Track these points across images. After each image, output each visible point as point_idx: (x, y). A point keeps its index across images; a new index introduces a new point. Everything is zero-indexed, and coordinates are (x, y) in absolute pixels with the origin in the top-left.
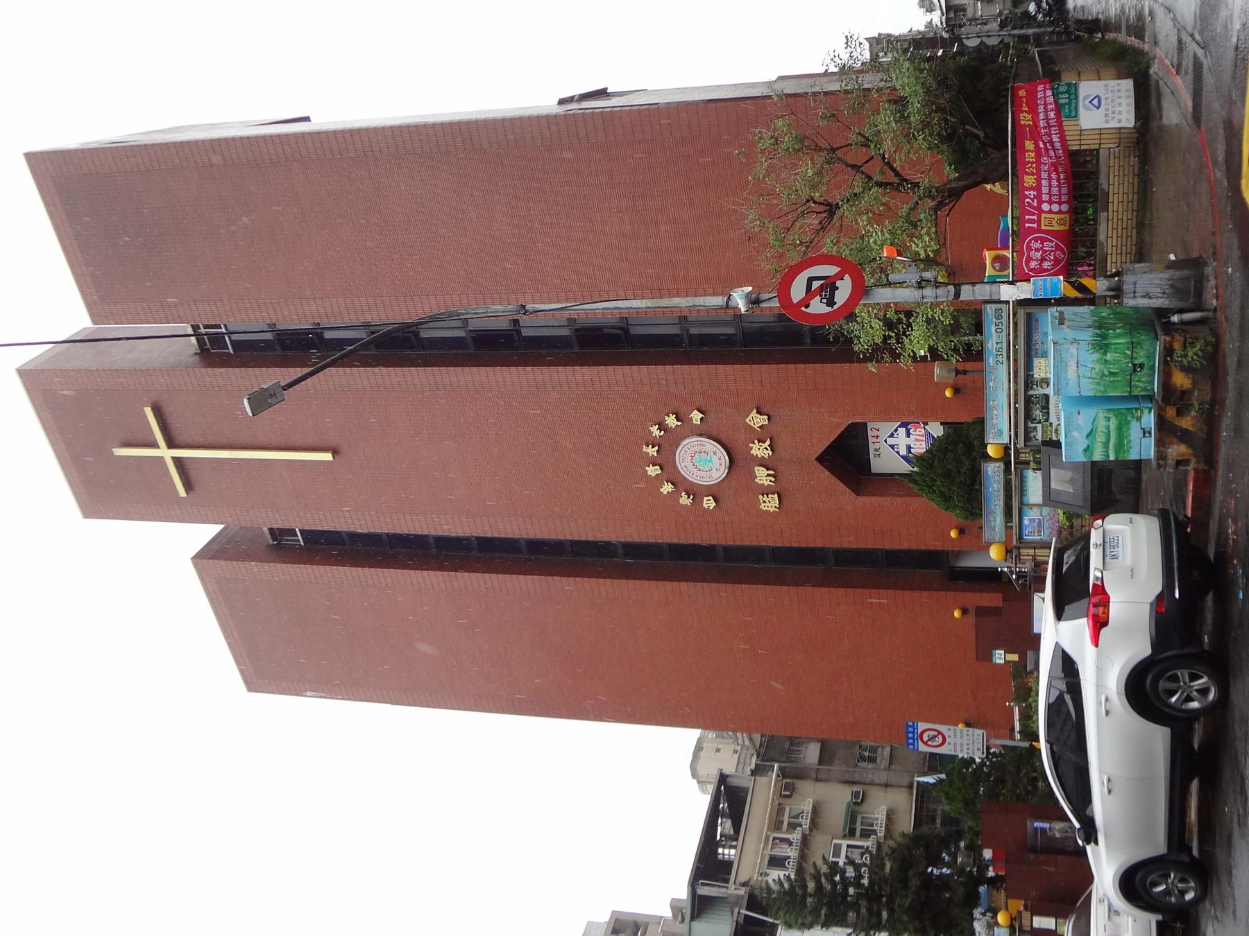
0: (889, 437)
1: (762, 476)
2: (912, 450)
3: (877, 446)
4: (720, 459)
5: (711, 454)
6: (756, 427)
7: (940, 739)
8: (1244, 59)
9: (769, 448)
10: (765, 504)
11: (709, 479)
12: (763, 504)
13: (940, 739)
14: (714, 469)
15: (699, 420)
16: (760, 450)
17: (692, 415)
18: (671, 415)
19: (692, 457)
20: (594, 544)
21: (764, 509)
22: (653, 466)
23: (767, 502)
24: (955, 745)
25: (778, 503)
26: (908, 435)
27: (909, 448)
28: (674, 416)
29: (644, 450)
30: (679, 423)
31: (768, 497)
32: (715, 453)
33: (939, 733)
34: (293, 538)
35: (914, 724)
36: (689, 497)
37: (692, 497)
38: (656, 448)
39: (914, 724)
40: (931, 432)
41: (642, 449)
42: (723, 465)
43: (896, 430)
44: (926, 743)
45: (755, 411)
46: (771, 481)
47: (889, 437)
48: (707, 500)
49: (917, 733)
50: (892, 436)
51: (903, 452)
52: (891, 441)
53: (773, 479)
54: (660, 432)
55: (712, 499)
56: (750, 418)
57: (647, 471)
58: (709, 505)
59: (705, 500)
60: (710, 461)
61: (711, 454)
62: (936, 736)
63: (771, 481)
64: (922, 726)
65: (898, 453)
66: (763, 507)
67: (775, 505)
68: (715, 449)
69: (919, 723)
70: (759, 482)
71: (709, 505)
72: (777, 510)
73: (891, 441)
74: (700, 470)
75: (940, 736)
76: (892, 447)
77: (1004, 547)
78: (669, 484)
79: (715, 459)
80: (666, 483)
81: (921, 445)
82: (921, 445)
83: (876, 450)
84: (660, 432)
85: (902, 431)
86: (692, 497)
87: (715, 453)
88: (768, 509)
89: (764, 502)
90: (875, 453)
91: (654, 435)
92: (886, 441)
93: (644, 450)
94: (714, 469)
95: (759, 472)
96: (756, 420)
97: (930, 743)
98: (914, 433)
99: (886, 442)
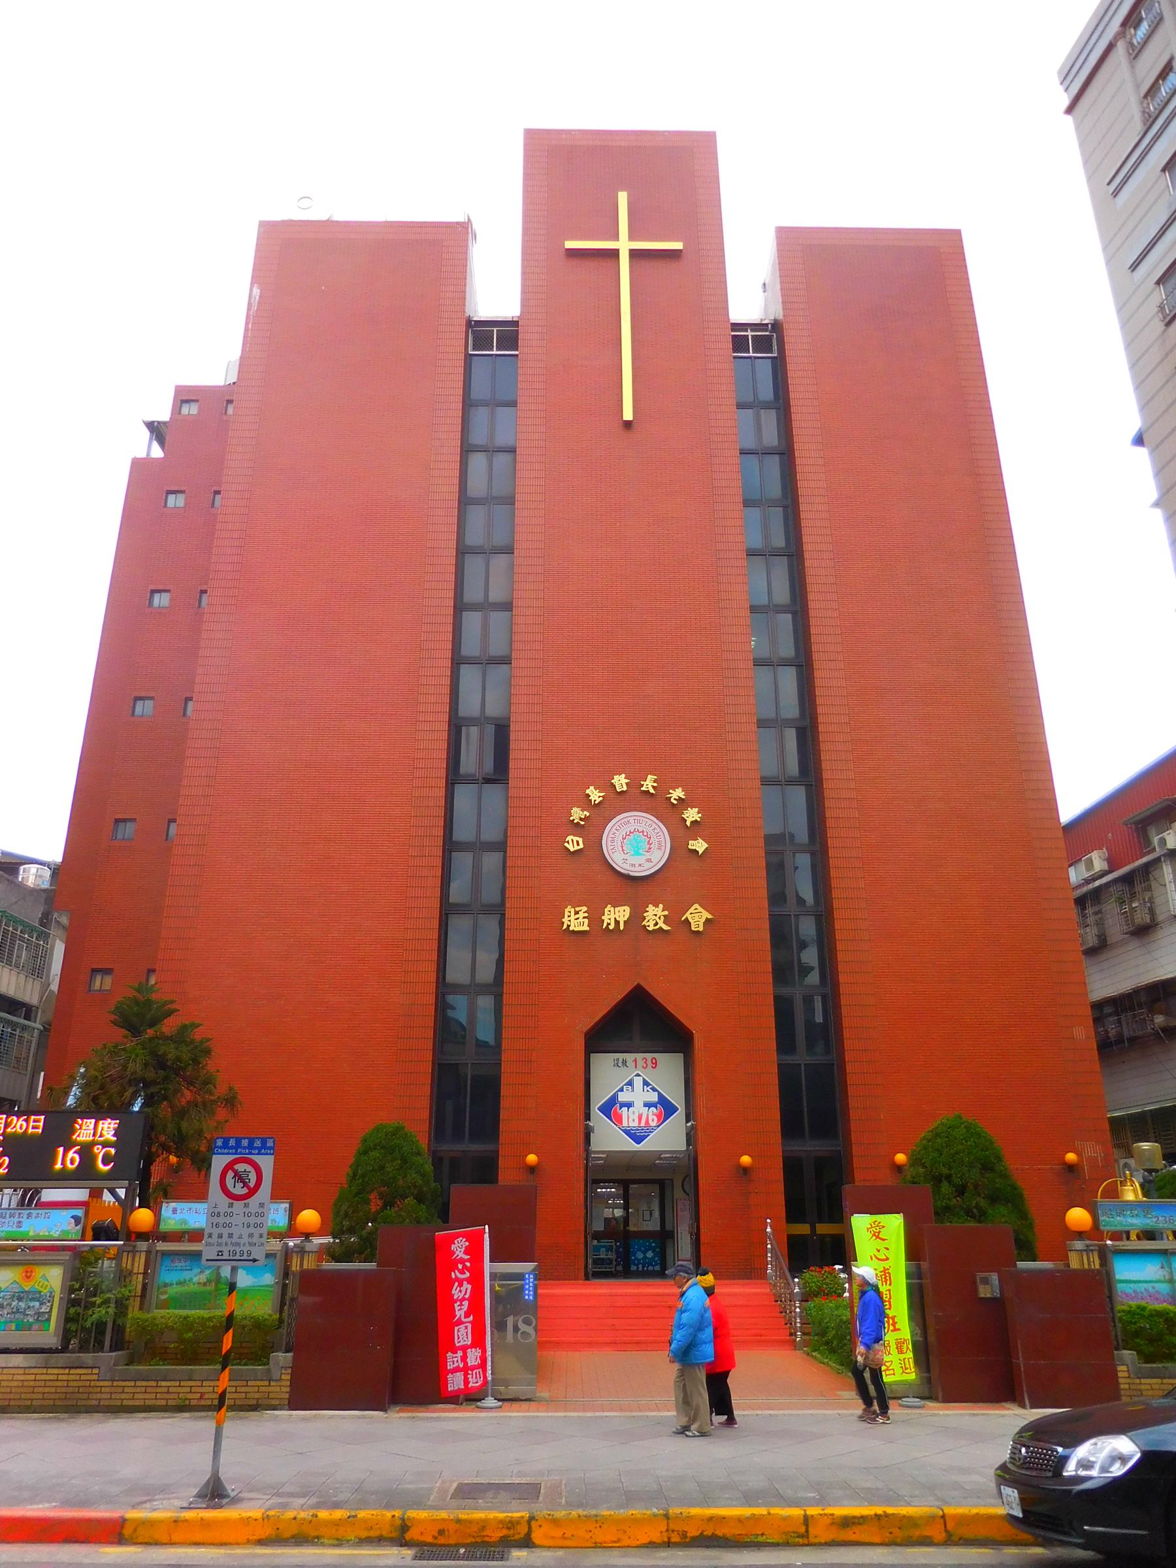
0: (643, 1079)
1: (616, 915)
2: (625, 1109)
3: (630, 1063)
4: (640, 865)
5: (648, 856)
6: (687, 915)
7: (239, 1190)
8: (596, 1543)
9: (657, 927)
10: (573, 913)
11: (610, 848)
12: (573, 911)
13: (239, 1190)
14: (626, 857)
15: (694, 848)
16: (654, 916)
17: (700, 840)
18: (700, 815)
19: (643, 832)
20: (812, 870)
21: (566, 910)
22: (627, 784)
23: (577, 916)
24: (231, 1215)
25: (576, 929)
26: (648, 1105)
27: (629, 1105)
28: (699, 820)
29: (650, 777)
30: (688, 823)
31: (584, 918)
32: (649, 860)
33: (252, 1192)
34: (1138, 853)
35: (270, 1148)
36: (581, 819)
37: (582, 823)
38: (652, 791)
39: (270, 1148)
40: (652, 1135)
41: (651, 774)
42: (633, 869)
43: (654, 1089)
44: (229, 1166)
45: (710, 916)
46: (609, 924)
47: (643, 1079)
48: (578, 842)
49: (250, 1153)
50: (646, 1083)
51: (622, 1097)
52: (638, 1082)
53: (611, 927)
54: (675, 799)
55: (579, 848)
56: (700, 909)
57: (620, 774)
58: (570, 842)
59: (578, 839)
60: (637, 853)
61: (648, 856)
62: (245, 1185)
63: (609, 924)
64: (266, 1163)
65: (621, 1090)
66: (569, 910)
67: (572, 925)
68: (655, 861)
69: (273, 1157)
70: (606, 910)
71: (570, 842)
72: (565, 927)
73: (638, 1082)
74: (623, 839)
75: (245, 1191)
76: (630, 1083)
77: (314, 1231)
78: (601, 798)
79: (637, 860)
80: (602, 794)
81: (634, 1120)
82: (634, 1120)
83: (624, 1063)
84: (675, 799)
85: (654, 1097)
86: (582, 823)
87: (649, 860)
88: (566, 916)
89: (577, 913)
90: (621, 1061)
91: (671, 791)
92: (638, 1075)
93: (650, 777)
94: (626, 857)
95: (622, 911)
96: (697, 917)
97: (230, 1174)
98: (650, 1113)
99: (636, 1076)
